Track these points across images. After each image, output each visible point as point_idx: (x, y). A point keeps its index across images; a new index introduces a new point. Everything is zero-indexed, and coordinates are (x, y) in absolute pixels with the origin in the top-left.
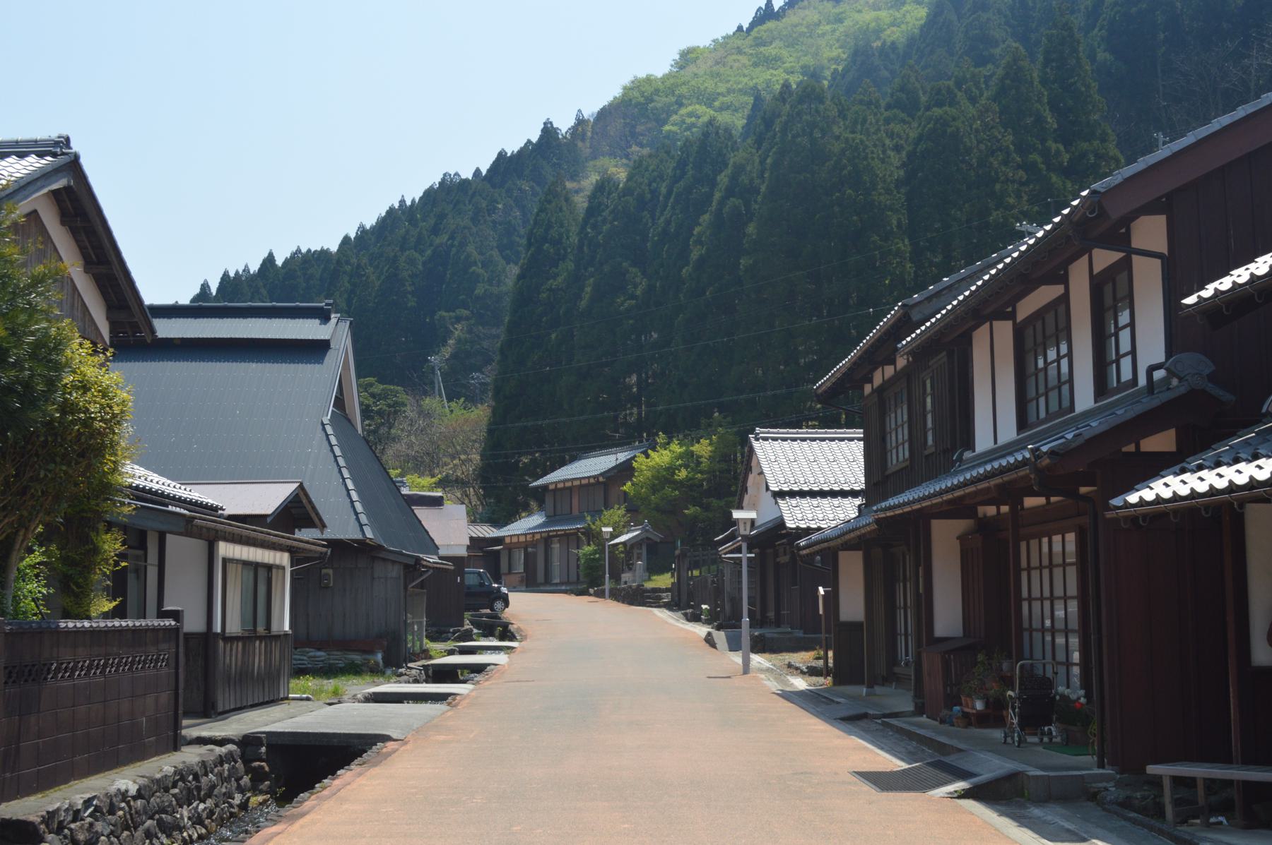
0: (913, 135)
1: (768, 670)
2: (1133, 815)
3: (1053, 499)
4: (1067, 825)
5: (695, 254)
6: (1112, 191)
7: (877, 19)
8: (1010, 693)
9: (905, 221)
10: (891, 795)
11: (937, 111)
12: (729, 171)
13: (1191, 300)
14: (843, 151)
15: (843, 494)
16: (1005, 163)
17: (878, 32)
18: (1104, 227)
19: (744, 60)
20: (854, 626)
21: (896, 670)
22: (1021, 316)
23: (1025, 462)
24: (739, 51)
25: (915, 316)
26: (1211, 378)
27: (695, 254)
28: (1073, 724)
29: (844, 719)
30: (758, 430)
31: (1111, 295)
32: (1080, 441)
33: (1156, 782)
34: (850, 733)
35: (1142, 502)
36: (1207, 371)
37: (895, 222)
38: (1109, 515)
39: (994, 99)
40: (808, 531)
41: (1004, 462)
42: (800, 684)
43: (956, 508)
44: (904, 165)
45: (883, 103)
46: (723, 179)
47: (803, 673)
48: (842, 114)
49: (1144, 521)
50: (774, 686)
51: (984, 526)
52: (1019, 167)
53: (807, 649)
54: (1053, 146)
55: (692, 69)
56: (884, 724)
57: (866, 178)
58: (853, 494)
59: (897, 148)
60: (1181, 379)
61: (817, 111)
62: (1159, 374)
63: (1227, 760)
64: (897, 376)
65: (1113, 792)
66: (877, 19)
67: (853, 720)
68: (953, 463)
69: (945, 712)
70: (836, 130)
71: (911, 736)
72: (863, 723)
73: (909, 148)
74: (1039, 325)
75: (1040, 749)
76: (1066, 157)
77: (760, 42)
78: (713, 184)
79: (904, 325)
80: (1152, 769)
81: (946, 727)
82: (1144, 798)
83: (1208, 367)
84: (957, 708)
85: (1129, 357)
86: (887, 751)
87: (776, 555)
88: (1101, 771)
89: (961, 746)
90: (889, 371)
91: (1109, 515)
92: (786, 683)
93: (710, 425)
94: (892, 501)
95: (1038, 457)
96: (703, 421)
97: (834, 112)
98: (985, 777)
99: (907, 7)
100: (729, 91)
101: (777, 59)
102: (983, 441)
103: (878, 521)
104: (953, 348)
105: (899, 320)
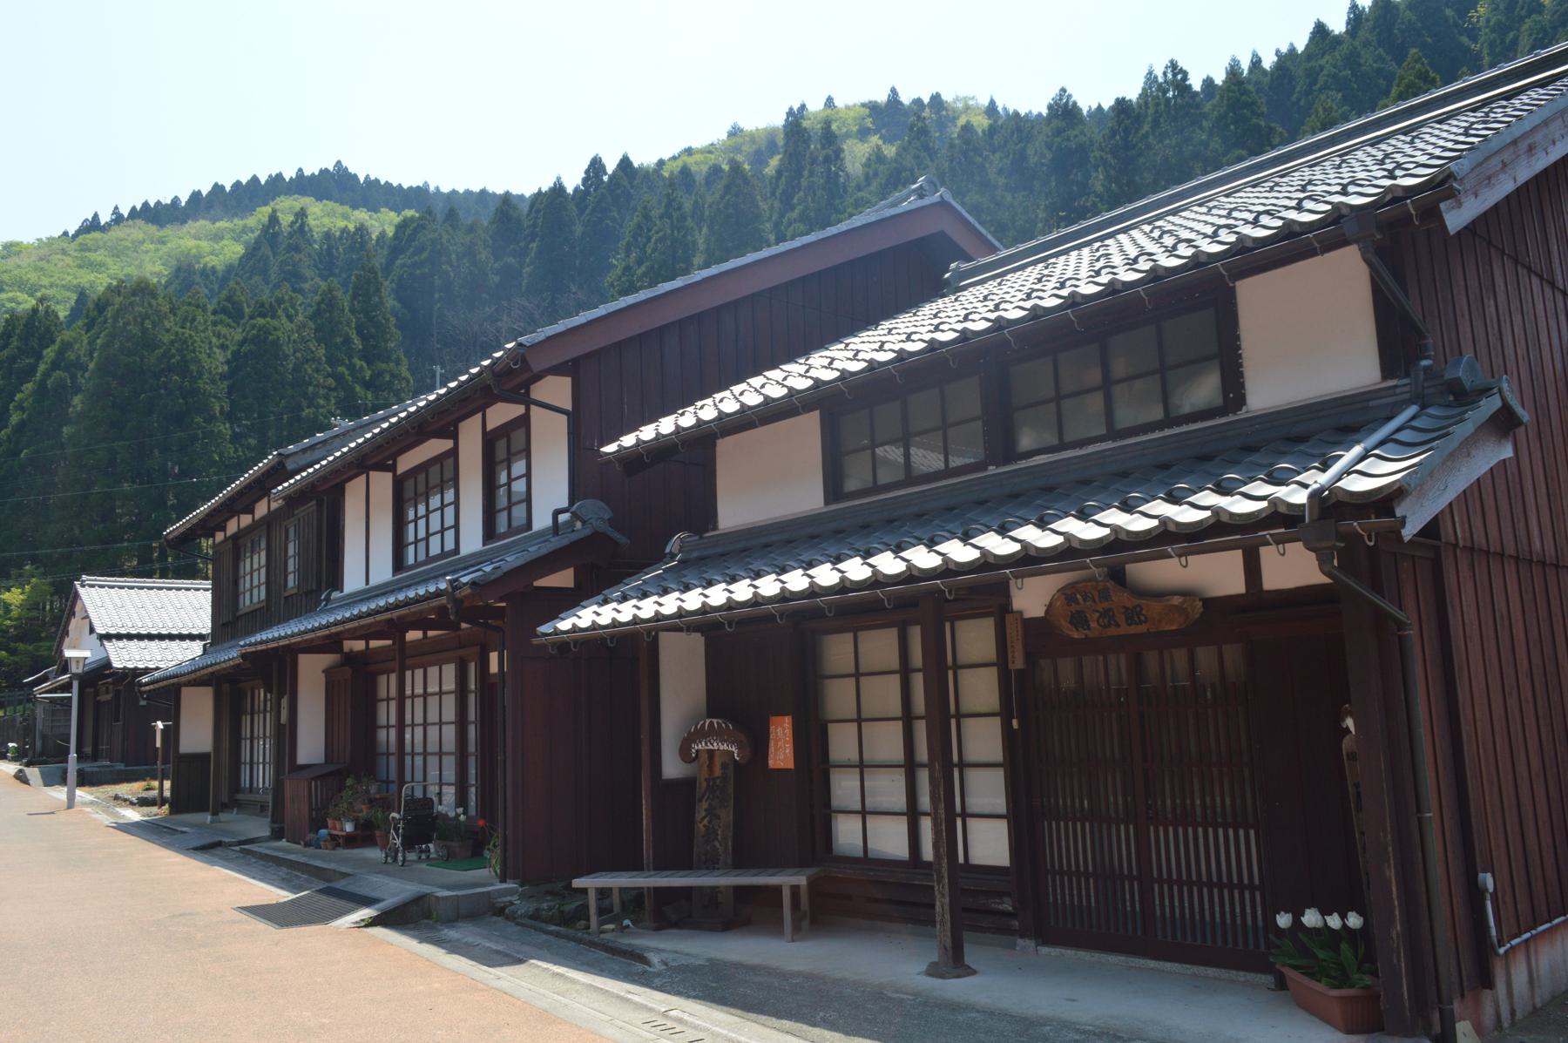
0: (238, 337)
1: (92, 803)
2: (553, 928)
3: (431, 633)
4: (493, 946)
5: (15, 419)
6: (534, 346)
7: (198, 247)
8: (394, 815)
9: (227, 409)
10: (293, 930)
11: (261, 321)
12: (56, 347)
13: (611, 448)
14: (172, 342)
15: (192, 637)
16: (317, 370)
17: (199, 257)
18: (514, 381)
19: (69, 260)
20: (200, 759)
21: (239, 796)
22: (401, 470)
23: (438, 594)
24: (64, 252)
25: (290, 466)
26: (611, 522)
27: (15, 419)
28: (467, 844)
29: (196, 849)
30: (84, 577)
31: (505, 448)
32: (499, 573)
33: (584, 891)
34: (212, 863)
35: (575, 629)
36: (606, 517)
37: (217, 408)
38: (535, 641)
39: (312, 318)
40: (147, 671)
41: (411, 594)
42: (133, 815)
43: (329, 643)
44: (228, 362)
45: (210, 308)
46: (49, 353)
47: (132, 804)
48: (173, 311)
49: (730, 625)
50: (106, 819)
51: (350, 659)
52: (329, 375)
53: (136, 780)
54: (358, 363)
55: (14, 261)
56: (242, 851)
57: (193, 367)
58: (201, 637)
59: (223, 347)
60: (584, 523)
61: (150, 305)
62: (563, 518)
63: (636, 866)
64: (255, 525)
65: (522, 907)
66: (198, 247)
67: (209, 849)
68: (318, 603)
69: (310, 836)
70: (168, 325)
71: (278, 862)
72: (218, 851)
73: (233, 348)
74: (422, 477)
75: (424, 866)
76: (368, 374)
77: (84, 248)
78: (39, 357)
79: (279, 472)
80: (578, 883)
81: (311, 850)
82: (550, 909)
83: (607, 515)
84: (323, 832)
85: (524, 505)
86: (261, 880)
87: (97, 693)
88: (504, 886)
89: (343, 869)
90: (246, 520)
91: (535, 641)
92: (116, 815)
93: (21, 575)
94: (258, 637)
95: (455, 588)
96: (14, 572)
97: (166, 308)
98: (389, 902)
99: (225, 242)
100: (52, 286)
101: (102, 264)
102: (353, 581)
103: (243, 656)
104: (325, 500)
105: (273, 468)
